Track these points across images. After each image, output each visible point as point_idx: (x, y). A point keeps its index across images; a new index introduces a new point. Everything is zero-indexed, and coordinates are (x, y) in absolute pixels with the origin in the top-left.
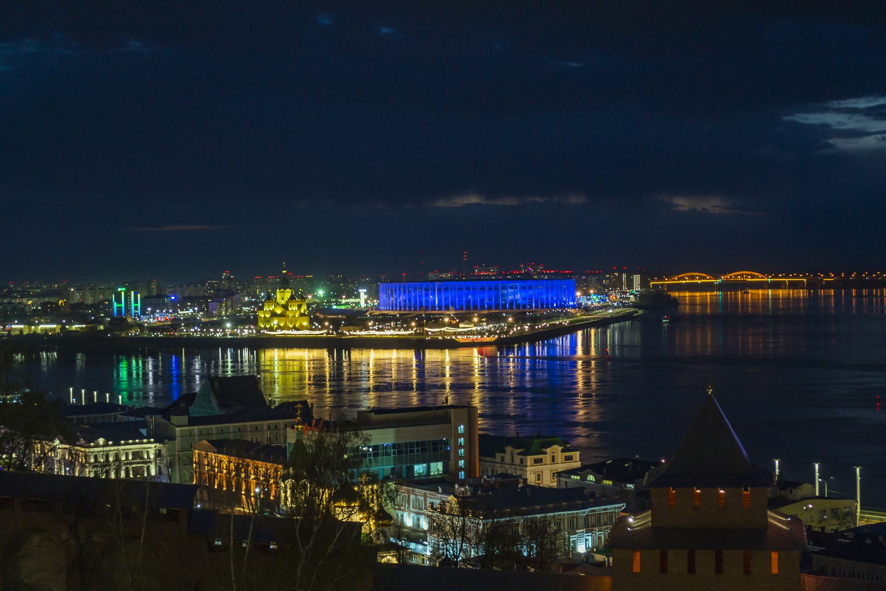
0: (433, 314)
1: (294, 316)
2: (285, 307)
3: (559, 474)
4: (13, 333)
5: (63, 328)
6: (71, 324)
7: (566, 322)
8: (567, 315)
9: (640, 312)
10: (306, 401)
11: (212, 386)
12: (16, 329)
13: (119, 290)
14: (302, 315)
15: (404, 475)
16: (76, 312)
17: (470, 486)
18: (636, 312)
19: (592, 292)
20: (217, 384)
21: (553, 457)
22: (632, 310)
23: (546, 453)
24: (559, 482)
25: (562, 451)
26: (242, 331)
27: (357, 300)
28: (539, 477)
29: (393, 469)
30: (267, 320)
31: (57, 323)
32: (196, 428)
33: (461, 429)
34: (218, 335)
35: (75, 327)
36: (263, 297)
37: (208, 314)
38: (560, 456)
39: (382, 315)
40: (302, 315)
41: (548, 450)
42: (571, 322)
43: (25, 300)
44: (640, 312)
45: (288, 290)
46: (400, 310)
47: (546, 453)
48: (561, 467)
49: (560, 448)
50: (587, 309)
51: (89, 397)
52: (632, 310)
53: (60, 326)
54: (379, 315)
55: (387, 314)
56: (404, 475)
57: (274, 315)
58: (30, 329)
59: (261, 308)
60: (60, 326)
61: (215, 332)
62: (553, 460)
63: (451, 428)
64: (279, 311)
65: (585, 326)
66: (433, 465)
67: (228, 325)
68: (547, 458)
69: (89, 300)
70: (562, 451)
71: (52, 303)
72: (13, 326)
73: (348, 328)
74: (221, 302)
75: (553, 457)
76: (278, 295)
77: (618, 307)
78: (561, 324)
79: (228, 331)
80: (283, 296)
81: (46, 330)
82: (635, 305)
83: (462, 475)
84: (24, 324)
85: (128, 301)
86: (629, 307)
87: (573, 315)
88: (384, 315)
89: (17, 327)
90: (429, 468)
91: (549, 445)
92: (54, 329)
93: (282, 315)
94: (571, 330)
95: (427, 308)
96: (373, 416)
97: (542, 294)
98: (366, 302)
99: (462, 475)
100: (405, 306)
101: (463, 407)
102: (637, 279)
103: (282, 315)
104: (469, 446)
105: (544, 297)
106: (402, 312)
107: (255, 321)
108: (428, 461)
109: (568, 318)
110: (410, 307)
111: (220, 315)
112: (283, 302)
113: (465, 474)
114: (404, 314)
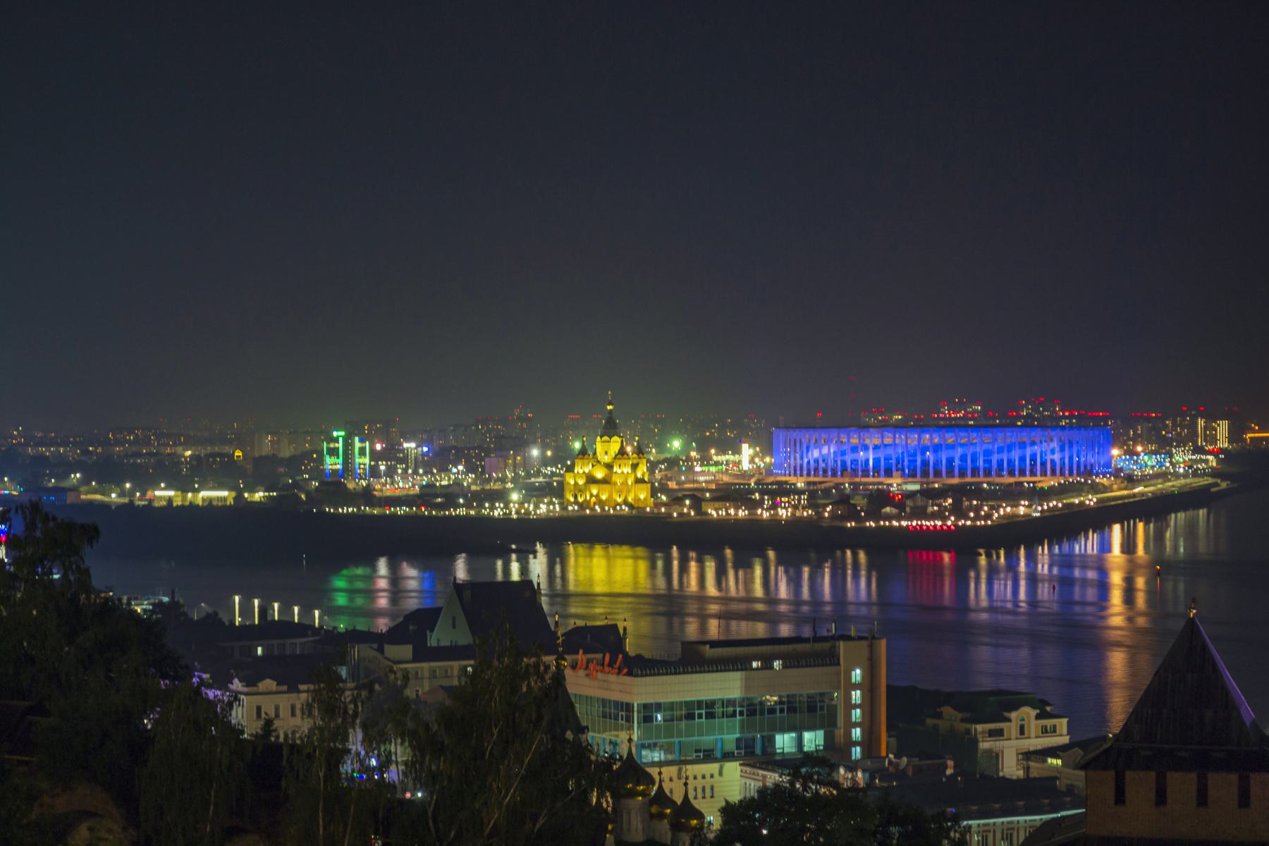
0: (865, 484)
1: (625, 483)
2: (609, 466)
3: (1027, 755)
4: (156, 504)
5: (239, 498)
6: (252, 491)
7: (1091, 500)
8: (1095, 489)
9: (1224, 485)
10: (616, 626)
11: (461, 600)
12: (161, 498)
13: (335, 434)
14: (639, 481)
15: (758, 751)
16: (262, 471)
17: (864, 771)
18: (1216, 485)
19: (1139, 449)
20: (467, 594)
21: (1022, 728)
22: (1210, 480)
23: (1009, 720)
24: (1027, 769)
25: (1038, 717)
26: (537, 507)
27: (736, 458)
28: (1202, 798)
29: (738, 740)
30: (578, 490)
31: (230, 489)
32: (425, 665)
33: (857, 675)
34: (496, 513)
35: (259, 496)
36: (686, 448)
37: (482, 477)
38: (1034, 725)
39: (778, 483)
40: (639, 481)
41: (1013, 715)
42: (1099, 501)
43: (179, 449)
44: (1224, 485)
45: (616, 438)
46: (809, 474)
47: (1009, 720)
48: (1036, 743)
49: (1033, 713)
50: (1131, 480)
51: (264, 611)
52: (1210, 480)
53: (233, 494)
54: (772, 484)
55: (786, 483)
56: (758, 751)
57: (591, 480)
58: (184, 499)
59: (570, 469)
60: (233, 494)
61: (492, 508)
62: (1022, 732)
63: (838, 674)
64: (600, 474)
65: (1125, 512)
66: (807, 736)
67: (515, 496)
68: (1011, 728)
69: (287, 452)
70: (1038, 717)
71: (222, 455)
72: (158, 493)
73: (717, 505)
74: (506, 457)
75: (1022, 728)
76: (599, 447)
77: (1185, 476)
78: (1082, 503)
79: (514, 508)
80: (607, 448)
81: (211, 500)
82: (1215, 473)
83: (857, 752)
84: (176, 489)
85: (349, 454)
86: (1204, 474)
87: (1106, 489)
88: (779, 483)
89: (163, 494)
90: (800, 741)
91: (1015, 707)
92: (225, 499)
93: (605, 481)
94: (1100, 519)
95: (855, 472)
96: (708, 651)
97: (1053, 452)
98: (752, 461)
99: (857, 752)
100: (816, 470)
101: (860, 638)
102: (1222, 428)
103: (605, 481)
104: (869, 705)
105: (1056, 457)
106: (811, 479)
107: (558, 491)
108: (799, 729)
109: (1096, 492)
110: (825, 471)
111: (503, 480)
112: (607, 459)
113: (863, 752)
114: (814, 483)
